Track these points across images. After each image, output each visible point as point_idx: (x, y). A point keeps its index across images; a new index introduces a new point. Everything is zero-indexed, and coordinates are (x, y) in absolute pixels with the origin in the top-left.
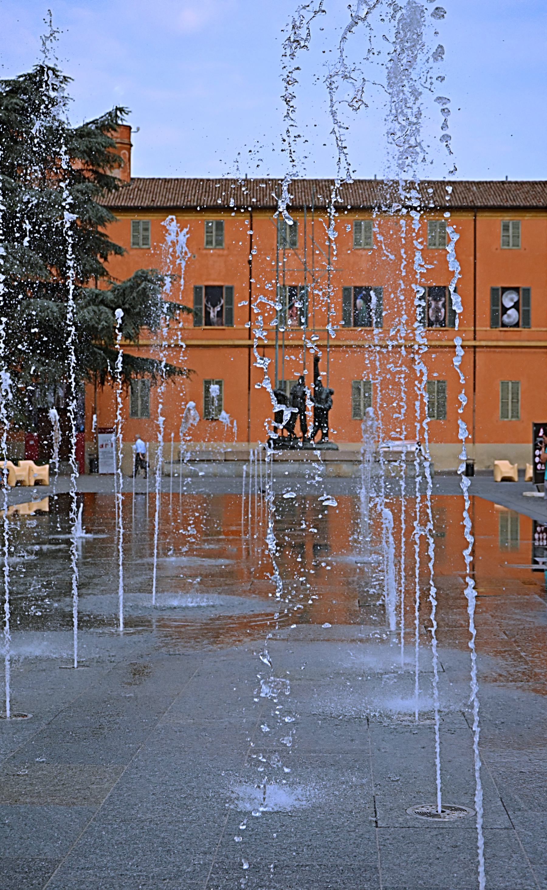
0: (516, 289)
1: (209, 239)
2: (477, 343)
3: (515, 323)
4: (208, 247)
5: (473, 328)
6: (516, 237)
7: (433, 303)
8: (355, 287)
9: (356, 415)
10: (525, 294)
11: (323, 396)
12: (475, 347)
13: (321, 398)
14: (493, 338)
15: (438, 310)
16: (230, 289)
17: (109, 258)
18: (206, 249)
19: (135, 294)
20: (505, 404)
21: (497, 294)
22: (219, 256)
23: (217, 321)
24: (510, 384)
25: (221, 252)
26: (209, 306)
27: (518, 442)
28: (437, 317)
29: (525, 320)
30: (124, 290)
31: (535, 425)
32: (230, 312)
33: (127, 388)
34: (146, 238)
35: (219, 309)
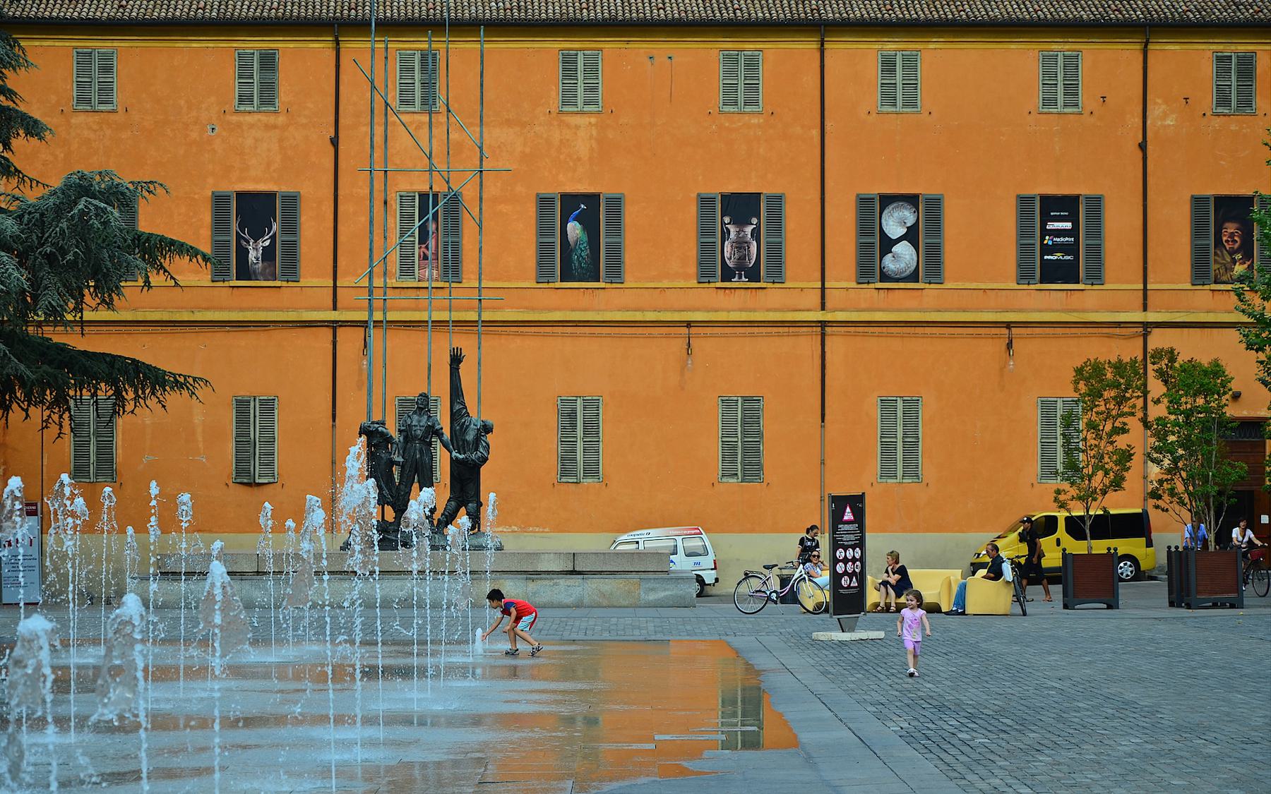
0: (911, 200)
1: (246, 90)
2: (828, 316)
3: (908, 273)
4: (242, 108)
5: (819, 285)
6: (911, 85)
7: (732, 229)
8: (564, 197)
9: (564, 473)
10: (930, 213)
11: (470, 436)
12: (823, 324)
13: (464, 441)
14: (863, 305)
15: (741, 245)
16: (292, 201)
17: (15, 143)
18: (237, 112)
19: (64, 225)
20: (888, 449)
21: (871, 208)
22: (268, 127)
23: (264, 269)
24: (900, 404)
25: (272, 119)
26: (247, 237)
27: (915, 529)
28: (742, 259)
29: (931, 266)
30: (42, 215)
31: (835, 499)
32: (292, 250)
33: (61, 417)
34: (106, 90)
35: (267, 243)
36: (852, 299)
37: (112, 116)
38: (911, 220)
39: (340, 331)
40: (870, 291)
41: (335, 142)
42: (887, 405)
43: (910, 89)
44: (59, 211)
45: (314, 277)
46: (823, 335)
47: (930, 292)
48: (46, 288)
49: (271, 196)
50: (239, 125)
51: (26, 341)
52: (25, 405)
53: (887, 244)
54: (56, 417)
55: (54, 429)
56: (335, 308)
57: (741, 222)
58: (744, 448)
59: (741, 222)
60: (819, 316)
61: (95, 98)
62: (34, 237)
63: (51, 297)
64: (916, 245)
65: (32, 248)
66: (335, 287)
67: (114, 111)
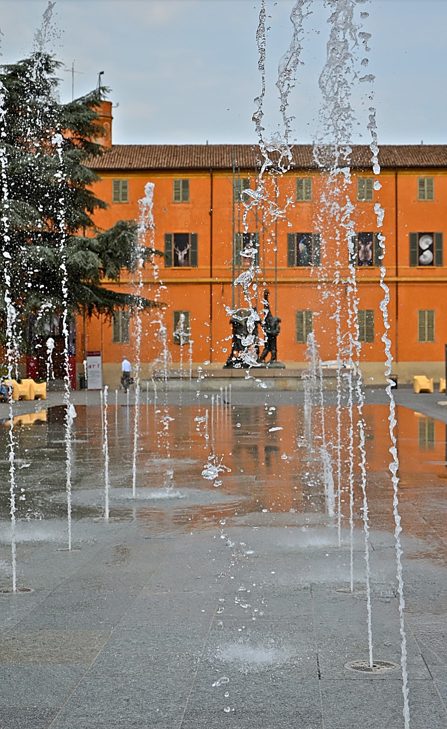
0: (431, 234)
1: (177, 195)
5: (395, 267)
6: (430, 190)
12: (397, 282)
14: (412, 275)
15: (365, 252)
16: (195, 236)
17: (95, 211)
18: (174, 203)
19: (116, 241)
20: (422, 329)
21: (415, 238)
22: (186, 209)
24: (426, 313)
25: (187, 206)
29: (438, 260)
30: (107, 238)
32: (195, 255)
33: (110, 318)
35: (186, 253)
36: (408, 272)
37: (127, 205)
39: (213, 286)
40: (415, 269)
41: (211, 214)
42: (422, 313)
43: (430, 192)
44: (114, 236)
45: (203, 265)
46: (397, 287)
47: (438, 269)
48: (109, 266)
49: (187, 235)
50: (175, 208)
52: (97, 314)
53: (421, 251)
54: (109, 319)
55: (108, 323)
56: (211, 277)
57: (365, 244)
58: (367, 330)
59: (365, 244)
60: (395, 279)
61: (121, 198)
62: (104, 247)
63: (112, 270)
64: (432, 252)
65: (103, 251)
66: (211, 269)
67: (128, 203)
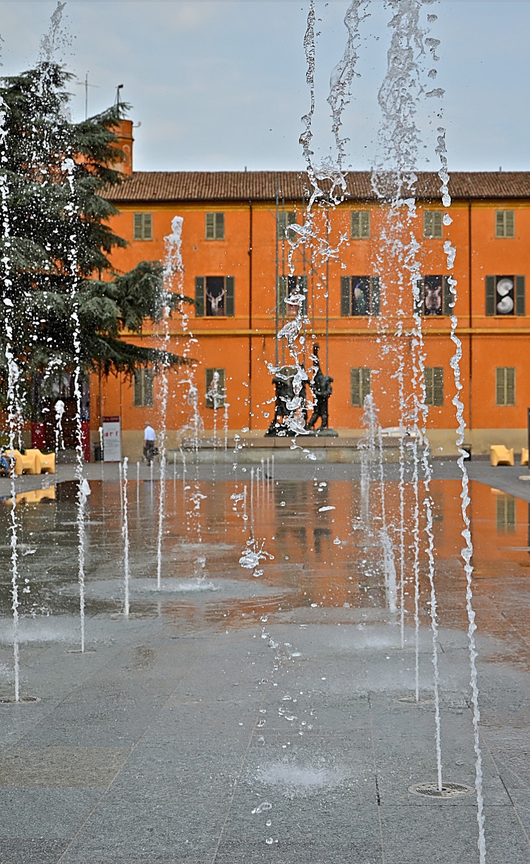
0: (511, 278)
1: (210, 231)
6: (510, 226)
7: (430, 292)
12: (471, 334)
14: (489, 326)
15: (433, 298)
16: (231, 280)
17: (112, 250)
18: (207, 241)
19: (137, 286)
20: (500, 390)
21: (492, 282)
22: (221, 247)
24: (506, 371)
25: (222, 244)
29: (520, 308)
30: (127, 282)
32: (231, 302)
33: (131, 377)
34: (148, 231)
35: (220, 299)
36: (484, 323)
37: (150, 243)
38: (510, 287)
40: (492, 319)
42: (500, 371)
44: (135, 280)
45: (241, 314)
46: (471, 340)
47: (519, 318)
48: (129, 315)
49: (222, 278)
50: (207, 246)
51: (115, 342)
52: (115, 372)
53: (500, 298)
54: (129, 378)
55: (128, 383)
57: (433, 289)
59: (433, 289)
60: (469, 331)
61: (143, 235)
63: (132, 319)
64: (513, 298)
65: (123, 298)
66: (250, 319)
67: (151, 241)
